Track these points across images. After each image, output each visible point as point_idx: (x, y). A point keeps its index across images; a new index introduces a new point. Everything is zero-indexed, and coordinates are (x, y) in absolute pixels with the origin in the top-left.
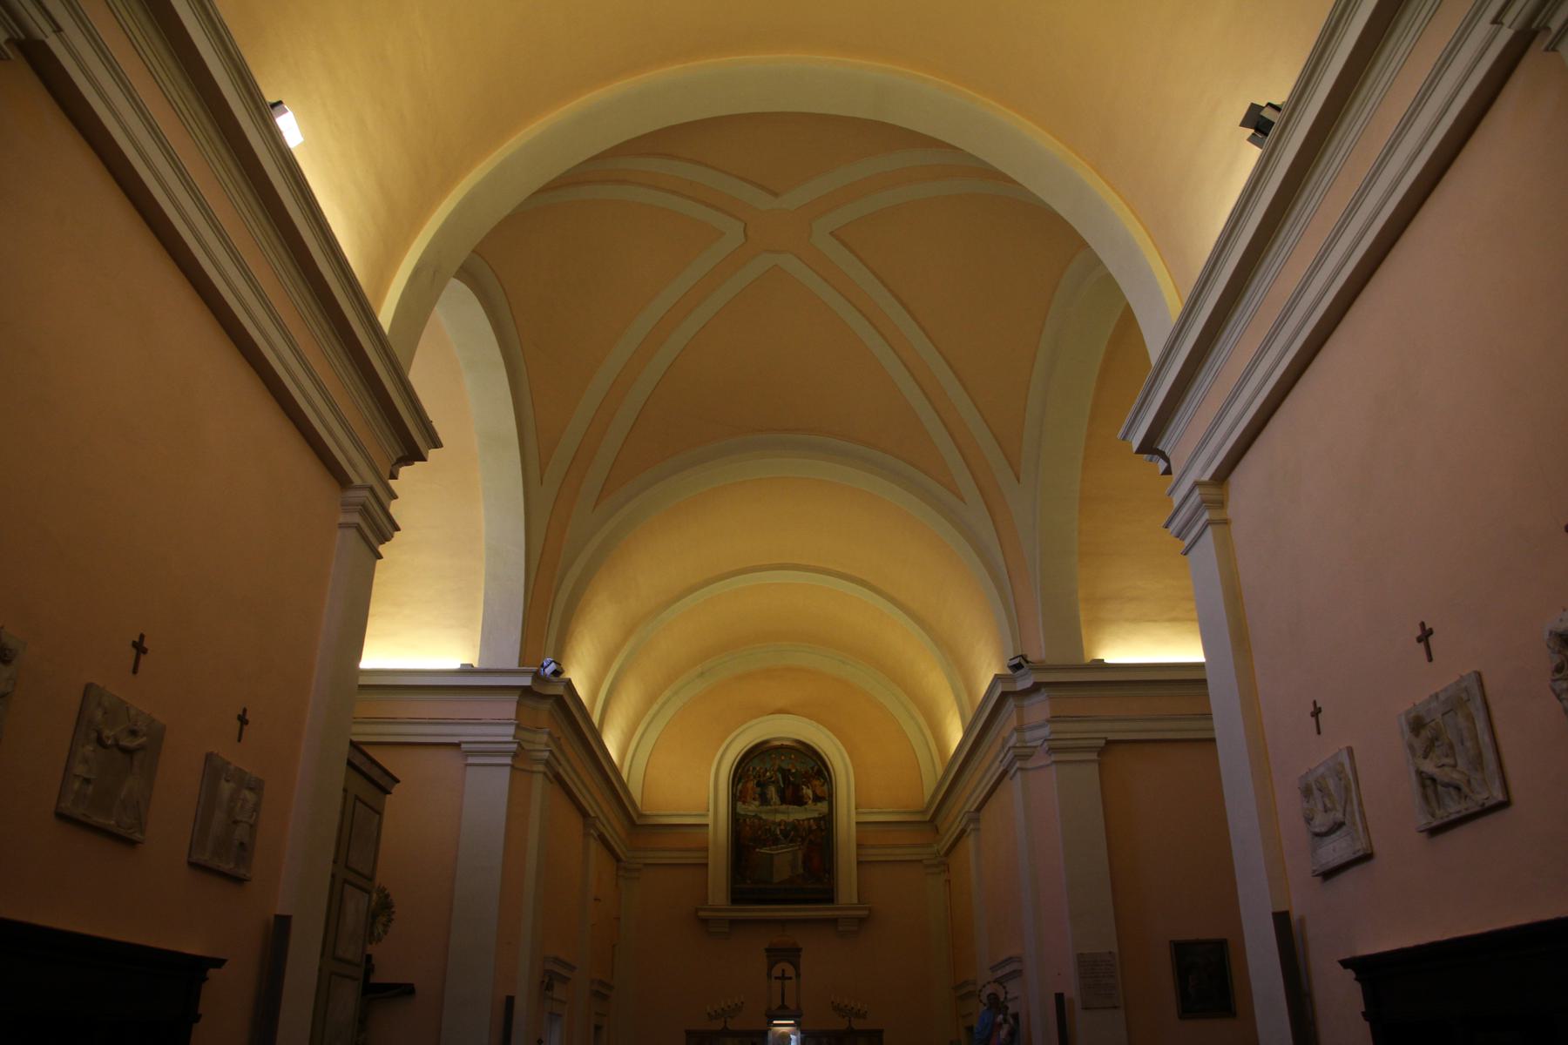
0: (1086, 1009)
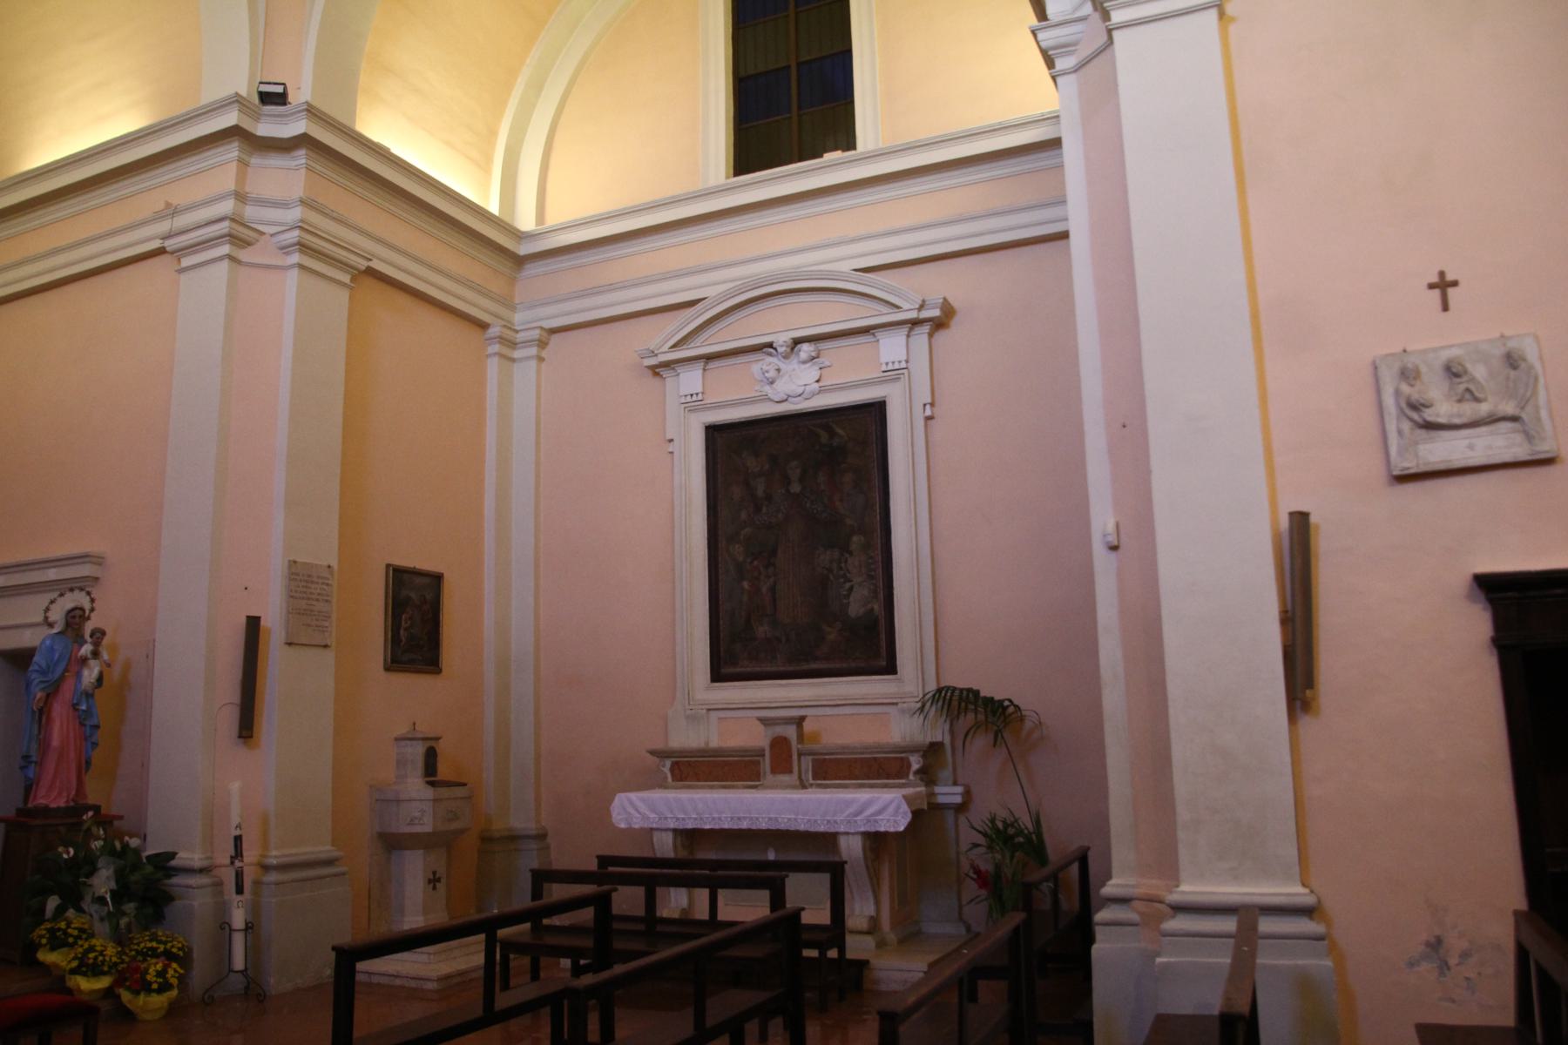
0: (290, 644)
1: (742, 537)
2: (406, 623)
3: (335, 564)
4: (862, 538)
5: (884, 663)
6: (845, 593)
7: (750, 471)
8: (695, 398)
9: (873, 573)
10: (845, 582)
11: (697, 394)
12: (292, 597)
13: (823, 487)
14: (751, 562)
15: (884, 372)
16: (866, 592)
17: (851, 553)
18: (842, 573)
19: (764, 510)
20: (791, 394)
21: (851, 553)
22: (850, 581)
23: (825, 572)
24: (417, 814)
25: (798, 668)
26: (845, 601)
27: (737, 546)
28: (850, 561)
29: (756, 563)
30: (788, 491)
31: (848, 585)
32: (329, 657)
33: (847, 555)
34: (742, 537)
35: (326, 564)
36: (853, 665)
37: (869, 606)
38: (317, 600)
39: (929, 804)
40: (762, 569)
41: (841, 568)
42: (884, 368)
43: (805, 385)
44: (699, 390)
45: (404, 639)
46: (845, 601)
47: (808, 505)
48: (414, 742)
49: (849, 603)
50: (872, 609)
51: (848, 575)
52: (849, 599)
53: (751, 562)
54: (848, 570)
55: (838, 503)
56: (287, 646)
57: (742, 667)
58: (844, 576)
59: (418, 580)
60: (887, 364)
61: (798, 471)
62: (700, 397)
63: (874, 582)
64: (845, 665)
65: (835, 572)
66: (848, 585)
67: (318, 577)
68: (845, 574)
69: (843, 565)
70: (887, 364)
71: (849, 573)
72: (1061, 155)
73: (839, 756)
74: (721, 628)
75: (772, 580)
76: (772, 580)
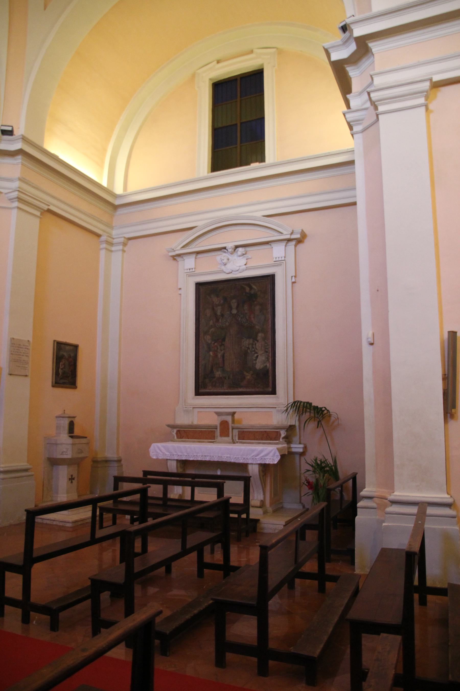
0: (11, 375)
2: (62, 366)
3: (31, 340)
5: (271, 390)
8: (191, 270)
9: (267, 350)
10: (254, 354)
12: (11, 354)
13: (246, 312)
14: (214, 344)
16: (264, 358)
17: (258, 341)
18: (253, 349)
19: (220, 321)
21: (258, 341)
22: (257, 353)
24: (65, 450)
26: (255, 362)
28: (257, 344)
29: (216, 344)
30: (231, 313)
31: (256, 355)
32: (28, 380)
33: (256, 342)
35: (26, 339)
37: (265, 365)
38: (23, 355)
40: (218, 347)
41: (253, 348)
42: (275, 260)
45: (61, 373)
46: (255, 362)
48: (64, 419)
49: (256, 363)
50: (266, 366)
51: (256, 350)
52: (256, 361)
53: (214, 344)
54: (256, 348)
55: (252, 319)
56: (9, 376)
58: (254, 351)
59: (68, 348)
61: (236, 304)
62: (193, 270)
63: (267, 354)
65: (251, 349)
66: (256, 355)
67: (23, 345)
69: (254, 346)
71: (257, 350)
72: (354, 168)
76: (223, 351)
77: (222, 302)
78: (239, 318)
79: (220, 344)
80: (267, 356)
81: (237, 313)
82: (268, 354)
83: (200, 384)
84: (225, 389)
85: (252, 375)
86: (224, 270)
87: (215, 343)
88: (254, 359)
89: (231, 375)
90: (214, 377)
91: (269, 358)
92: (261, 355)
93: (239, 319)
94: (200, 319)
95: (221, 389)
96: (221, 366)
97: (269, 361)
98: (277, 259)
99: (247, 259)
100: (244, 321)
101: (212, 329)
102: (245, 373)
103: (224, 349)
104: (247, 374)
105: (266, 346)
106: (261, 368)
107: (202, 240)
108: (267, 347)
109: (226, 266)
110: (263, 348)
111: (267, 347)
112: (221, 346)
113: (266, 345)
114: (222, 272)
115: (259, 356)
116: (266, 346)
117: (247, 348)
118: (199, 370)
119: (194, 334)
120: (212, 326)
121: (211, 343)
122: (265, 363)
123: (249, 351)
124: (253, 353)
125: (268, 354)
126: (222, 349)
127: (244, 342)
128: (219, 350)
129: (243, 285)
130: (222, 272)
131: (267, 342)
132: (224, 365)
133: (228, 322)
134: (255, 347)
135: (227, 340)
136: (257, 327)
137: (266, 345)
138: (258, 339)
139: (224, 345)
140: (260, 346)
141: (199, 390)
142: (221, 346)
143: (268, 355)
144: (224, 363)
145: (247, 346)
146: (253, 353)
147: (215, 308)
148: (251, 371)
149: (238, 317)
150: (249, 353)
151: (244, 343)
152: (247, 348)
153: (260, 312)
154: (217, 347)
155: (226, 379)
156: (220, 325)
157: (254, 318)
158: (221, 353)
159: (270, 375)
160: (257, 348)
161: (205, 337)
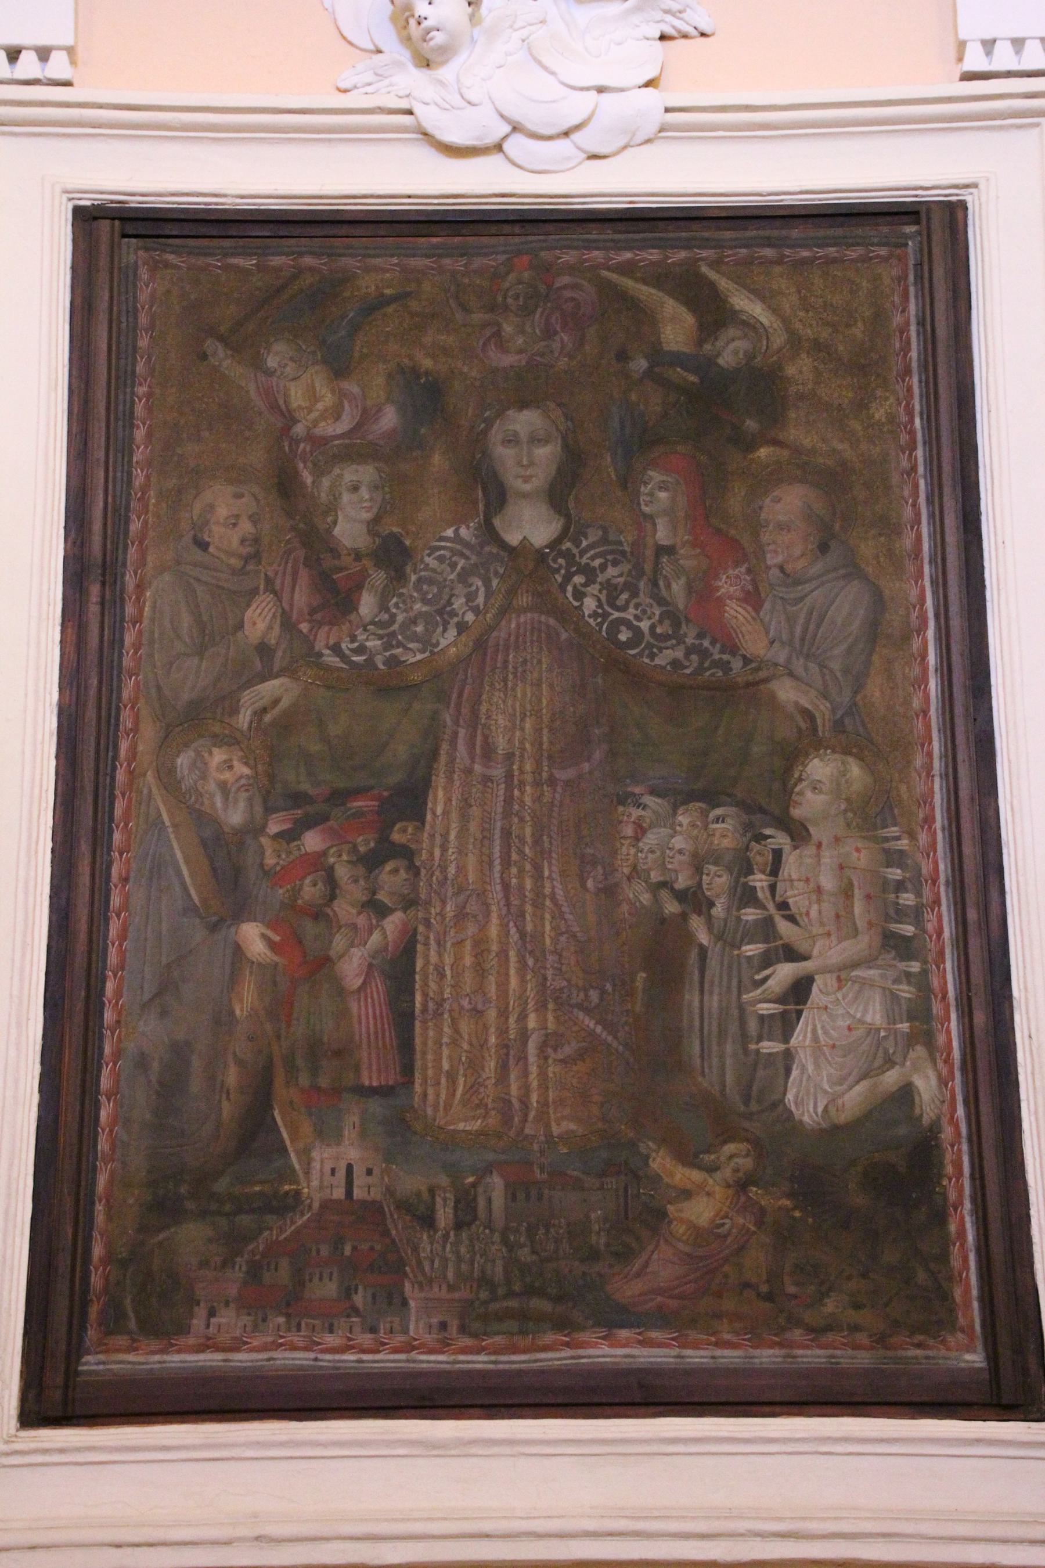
1: (244, 719)
4: (855, 770)
5: (975, 1359)
6: (766, 1008)
7: (299, 429)
8: (28, 66)
9: (908, 930)
10: (767, 961)
11: (44, 54)
13: (663, 534)
14: (290, 836)
15: (969, 76)
16: (875, 1014)
17: (799, 833)
18: (750, 914)
19: (367, 605)
20: (533, 118)
21: (799, 833)
22: (792, 954)
23: (672, 907)
25: (518, 1361)
26: (769, 1047)
27: (218, 756)
28: (792, 865)
29: (312, 841)
30: (490, 533)
31: (784, 973)
33: (781, 840)
34: (244, 719)
36: (812, 1357)
37: (891, 1078)
39: (468, 914)
40: (342, 872)
41: (748, 897)
42: (975, 61)
43: (601, 90)
44: (59, 34)
46: (769, 1047)
47: (590, 604)
49: (788, 1056)
50: (906, 1093)
51: (783, 926)
52: (786, 1036)
53: (290, 836)
54: (783, 906)
55: (736, 613)
57: (207, 1345)
58: (766, 929)
60: (988, 45)
61: (546, 454)
62: (58, 66)
63: (915, 967)
64: (767, 1357)
65: (718, 911)
66: (784, 973)
68: (768, 923)
69: (759, 881)
70: (988, 45)
71: (792, 919)
73: (596, 1360)
74: (103, 1144)
75: (393, 923)
76: (393, 923)
77: (389, 419)
78: (579, 595)
79: (365, 843)
80: (906, 991)
81: (554, 544)
82: (924, 972)
83: (96, 1280)
84: (409, 1347)
85: (742, 1185)
86: (429, 117)
87: (307, 823)
88: (762, 1018)
89: (497, 1181)
90: (292, 1203)
91: (936, 1008)
92: (842, 972)
93: (590, 604)
94: (78, 1092)
95: (366, 1339)
96: (369, 1078)
97: (941, 1039)
98: (1004, 59)
99: (663, 37)
100: (644, 625)
101: (272, 687)
102: (661, 1162)
103: (409, 903)
104: (682, 1175)
105: (900, 886)
106: (842, 1118)
107: (97, 897)
108: (908, 899)
109: (446, 73)
110: (858, 907)
111: (908, 899)
112: (371, 862)
113: (895, 874)
114: (404, 129)
115: (819, 981)
116: (900, 886)
117: (681, 896)
118: (87, 1121)
119: (52, 723)
120: (263, 649)
121: (254, 829)
122: (889, 1062)
123: (698, 927)
124: (751, 950)
125: (924, 972)
126: (382, 896)
127: (641, 830)
128: (344, 909)
129: (628, 283)
130: (404, 129)
131: (904, 844)
132: (408, 1070)
133: (462, 628)
134: (773, 888)
135: (438, 802)
136: (786, 692)
137: (895, 874)
138: (796, 812)
139: (407, 854)
140: (828, 881)
141: (75, 1351)
142: (371, 862)
143: (922, 983)
144: (406, 1046)
145: (682, 882)
146: (751, 950)
147: (308, 479)
148: (730, 1148)
149: (578, 579)
150: (703, 951)
151: (651, 839)
152: (681, 896)
153: (824, 548)
154: (330, 871)
155: (428, 1221)
156: (361, 650)
157: (753, 599)
158: (376, 937)
159: (952, 1196)
160: (797, 901)
161: (183, 761)
